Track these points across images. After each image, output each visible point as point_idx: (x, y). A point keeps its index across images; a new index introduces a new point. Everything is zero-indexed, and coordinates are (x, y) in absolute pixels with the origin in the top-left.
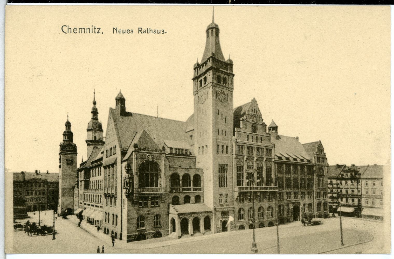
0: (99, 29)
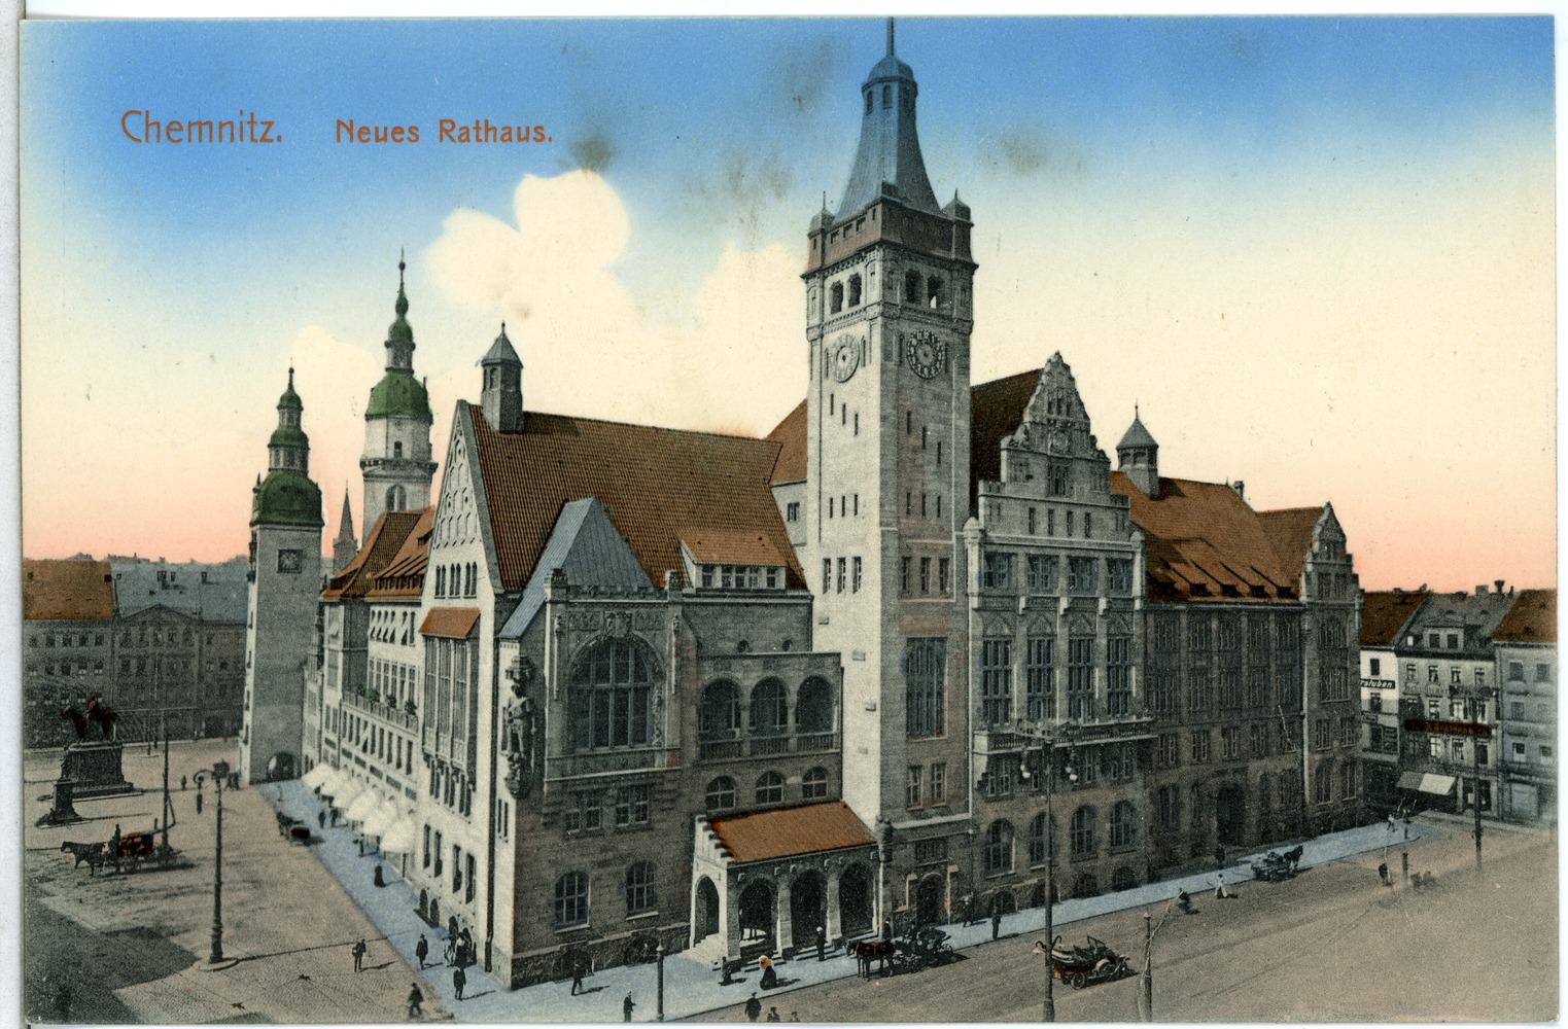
0: (270, 124)
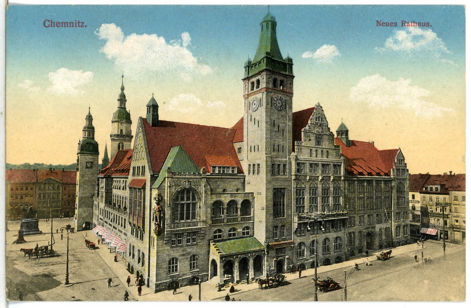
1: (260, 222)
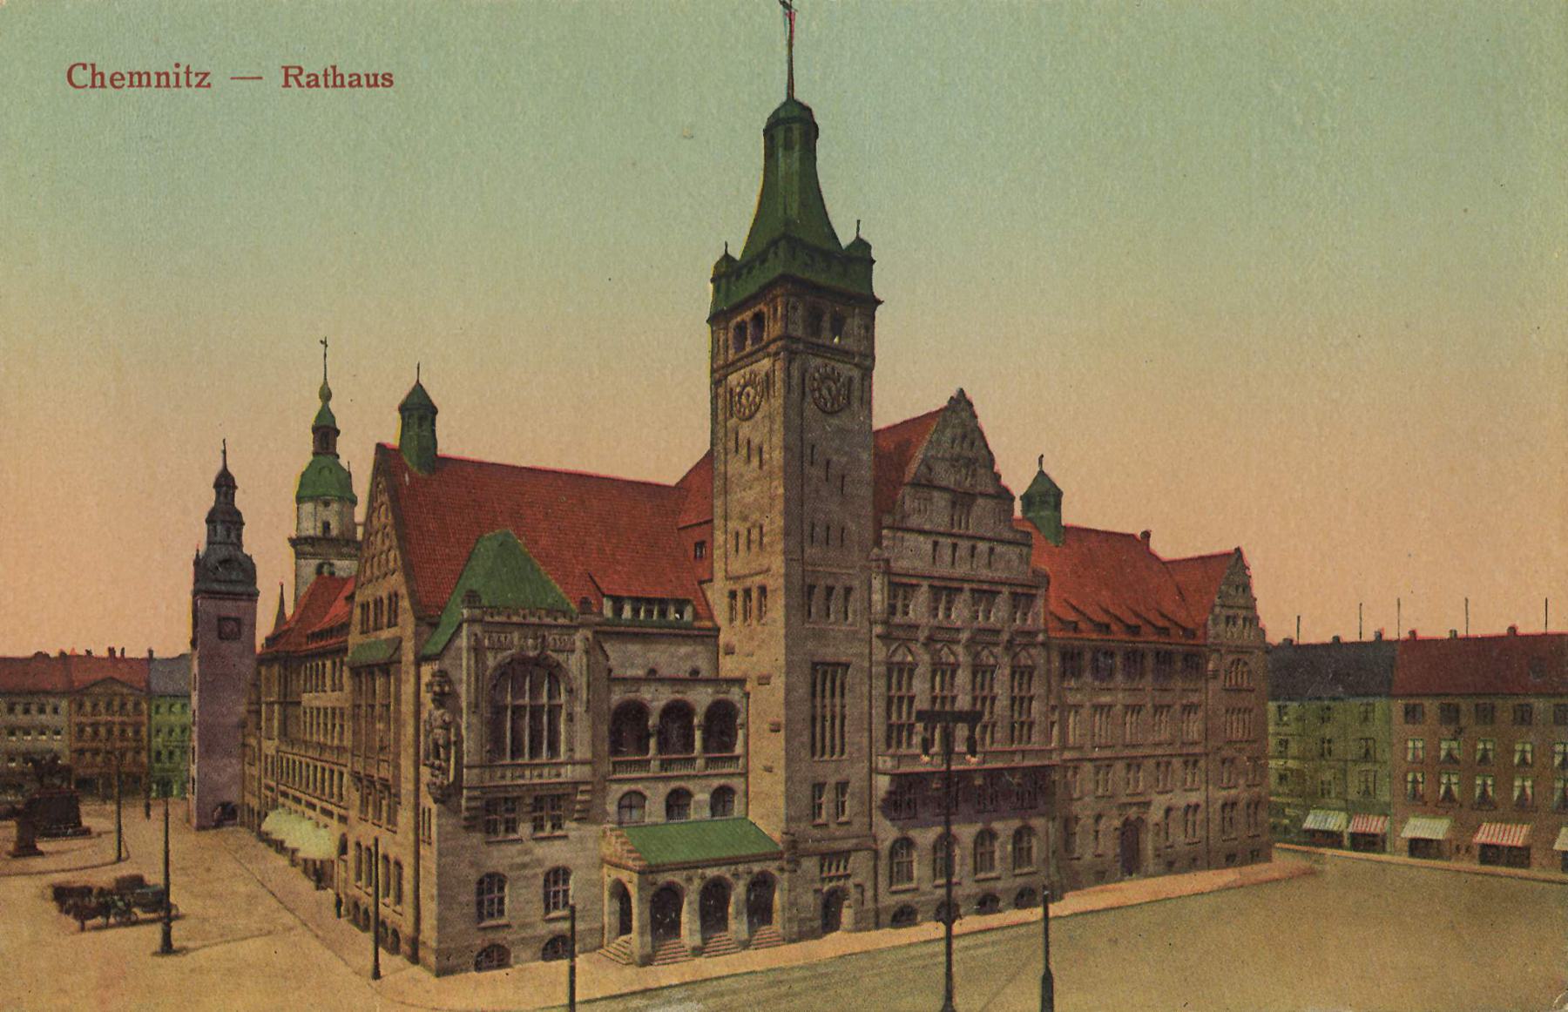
0: (206, 75)
1: (769, 770)
